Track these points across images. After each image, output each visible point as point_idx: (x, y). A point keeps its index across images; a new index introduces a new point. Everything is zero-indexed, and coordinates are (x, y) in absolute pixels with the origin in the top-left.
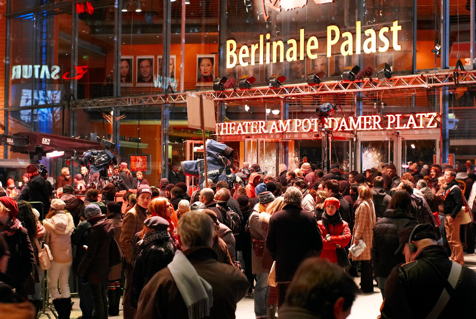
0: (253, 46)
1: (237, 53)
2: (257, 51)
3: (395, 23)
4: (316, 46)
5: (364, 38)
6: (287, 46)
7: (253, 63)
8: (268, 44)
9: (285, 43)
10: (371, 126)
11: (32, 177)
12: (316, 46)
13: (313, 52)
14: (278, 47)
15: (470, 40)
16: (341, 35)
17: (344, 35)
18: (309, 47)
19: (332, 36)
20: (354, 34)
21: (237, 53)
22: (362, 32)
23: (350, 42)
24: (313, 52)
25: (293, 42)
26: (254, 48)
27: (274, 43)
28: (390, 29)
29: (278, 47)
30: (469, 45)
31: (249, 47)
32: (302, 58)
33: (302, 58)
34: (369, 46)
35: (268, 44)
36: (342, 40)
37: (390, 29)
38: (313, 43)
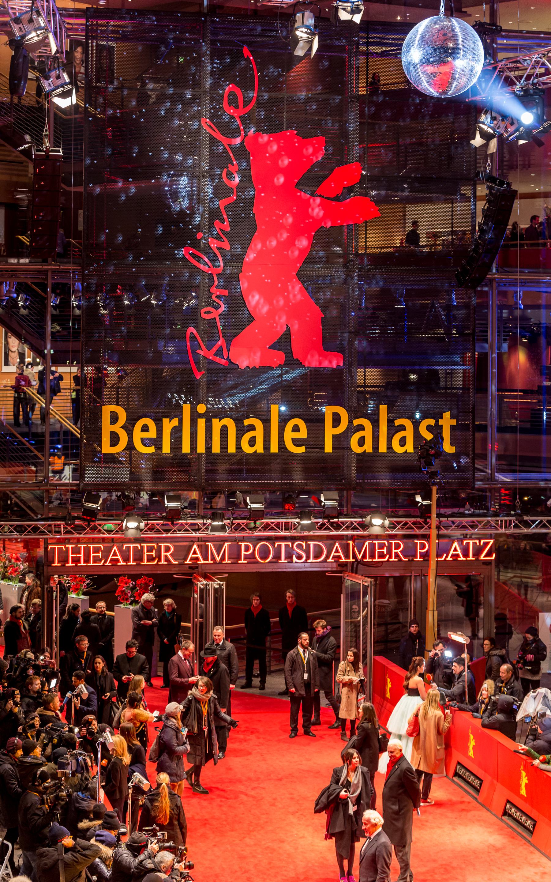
0: (165, 421)
1: (129, 428)
2: (177, 432)
3: (447, 415)
4: (303, 434)
5: (393, 429)
6: (241, 431)
7: (166, 448)
8: (201, 423)
9: (238, 421)
10: (388, 556)
11: (434, 293)
12: (303, 434)
13: (297, 442)
14: (224, 431)
15: (340, 607)
16: (351, 422)
17: (356, 422)
18: (289, 435)
19: (334, 421)
20: (376, 423)
21: (129, 428)
22: (390, 422)
23: (368, 433)
24: (297, 442)
25: (258, 423)
26: (168, 425)
27: (215, 421)
28: (437, 422)
29: (224, 431)
30: (340, 611)
31: (158, 422)
32: (274, 448)
33: (274, 448)
34: (403, 441)
35: (201, 423)
36: (352, 430)
37: (437, 422)
38: (296, 429)
